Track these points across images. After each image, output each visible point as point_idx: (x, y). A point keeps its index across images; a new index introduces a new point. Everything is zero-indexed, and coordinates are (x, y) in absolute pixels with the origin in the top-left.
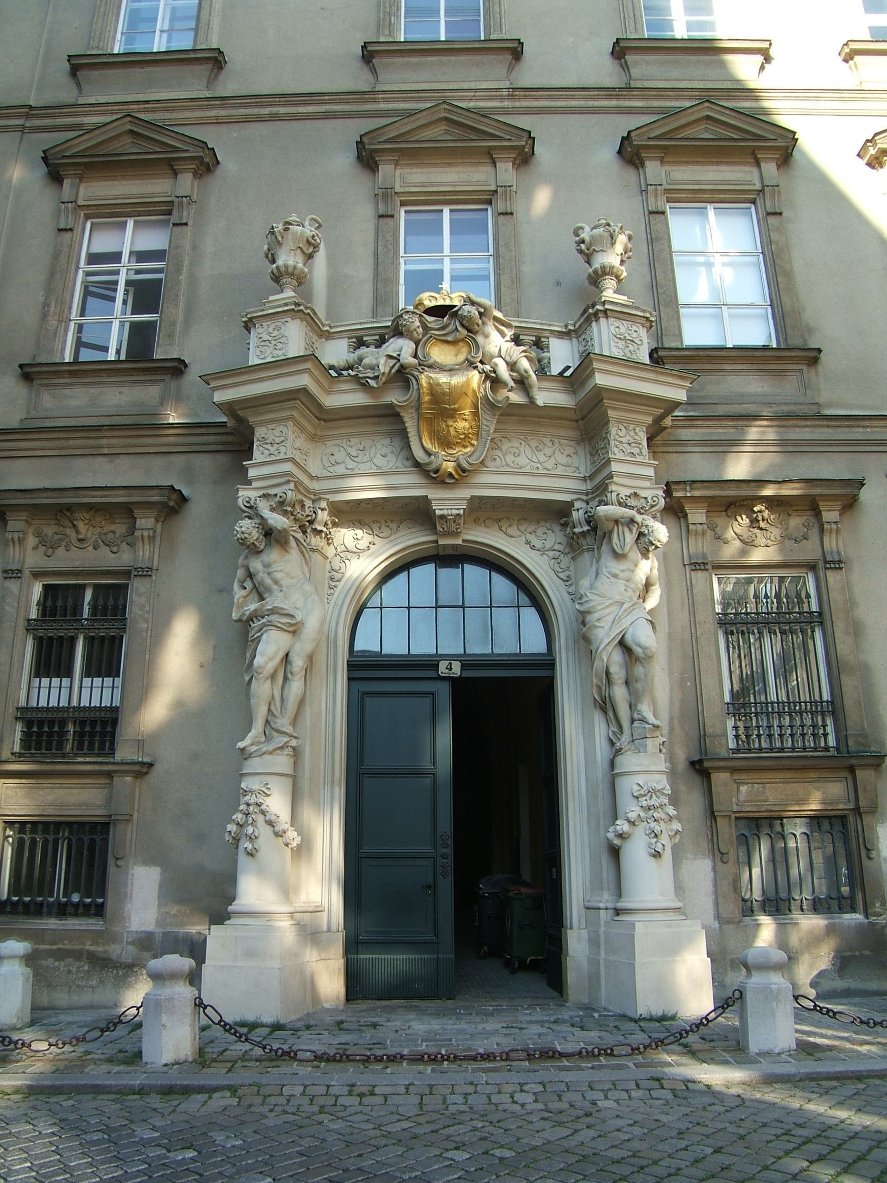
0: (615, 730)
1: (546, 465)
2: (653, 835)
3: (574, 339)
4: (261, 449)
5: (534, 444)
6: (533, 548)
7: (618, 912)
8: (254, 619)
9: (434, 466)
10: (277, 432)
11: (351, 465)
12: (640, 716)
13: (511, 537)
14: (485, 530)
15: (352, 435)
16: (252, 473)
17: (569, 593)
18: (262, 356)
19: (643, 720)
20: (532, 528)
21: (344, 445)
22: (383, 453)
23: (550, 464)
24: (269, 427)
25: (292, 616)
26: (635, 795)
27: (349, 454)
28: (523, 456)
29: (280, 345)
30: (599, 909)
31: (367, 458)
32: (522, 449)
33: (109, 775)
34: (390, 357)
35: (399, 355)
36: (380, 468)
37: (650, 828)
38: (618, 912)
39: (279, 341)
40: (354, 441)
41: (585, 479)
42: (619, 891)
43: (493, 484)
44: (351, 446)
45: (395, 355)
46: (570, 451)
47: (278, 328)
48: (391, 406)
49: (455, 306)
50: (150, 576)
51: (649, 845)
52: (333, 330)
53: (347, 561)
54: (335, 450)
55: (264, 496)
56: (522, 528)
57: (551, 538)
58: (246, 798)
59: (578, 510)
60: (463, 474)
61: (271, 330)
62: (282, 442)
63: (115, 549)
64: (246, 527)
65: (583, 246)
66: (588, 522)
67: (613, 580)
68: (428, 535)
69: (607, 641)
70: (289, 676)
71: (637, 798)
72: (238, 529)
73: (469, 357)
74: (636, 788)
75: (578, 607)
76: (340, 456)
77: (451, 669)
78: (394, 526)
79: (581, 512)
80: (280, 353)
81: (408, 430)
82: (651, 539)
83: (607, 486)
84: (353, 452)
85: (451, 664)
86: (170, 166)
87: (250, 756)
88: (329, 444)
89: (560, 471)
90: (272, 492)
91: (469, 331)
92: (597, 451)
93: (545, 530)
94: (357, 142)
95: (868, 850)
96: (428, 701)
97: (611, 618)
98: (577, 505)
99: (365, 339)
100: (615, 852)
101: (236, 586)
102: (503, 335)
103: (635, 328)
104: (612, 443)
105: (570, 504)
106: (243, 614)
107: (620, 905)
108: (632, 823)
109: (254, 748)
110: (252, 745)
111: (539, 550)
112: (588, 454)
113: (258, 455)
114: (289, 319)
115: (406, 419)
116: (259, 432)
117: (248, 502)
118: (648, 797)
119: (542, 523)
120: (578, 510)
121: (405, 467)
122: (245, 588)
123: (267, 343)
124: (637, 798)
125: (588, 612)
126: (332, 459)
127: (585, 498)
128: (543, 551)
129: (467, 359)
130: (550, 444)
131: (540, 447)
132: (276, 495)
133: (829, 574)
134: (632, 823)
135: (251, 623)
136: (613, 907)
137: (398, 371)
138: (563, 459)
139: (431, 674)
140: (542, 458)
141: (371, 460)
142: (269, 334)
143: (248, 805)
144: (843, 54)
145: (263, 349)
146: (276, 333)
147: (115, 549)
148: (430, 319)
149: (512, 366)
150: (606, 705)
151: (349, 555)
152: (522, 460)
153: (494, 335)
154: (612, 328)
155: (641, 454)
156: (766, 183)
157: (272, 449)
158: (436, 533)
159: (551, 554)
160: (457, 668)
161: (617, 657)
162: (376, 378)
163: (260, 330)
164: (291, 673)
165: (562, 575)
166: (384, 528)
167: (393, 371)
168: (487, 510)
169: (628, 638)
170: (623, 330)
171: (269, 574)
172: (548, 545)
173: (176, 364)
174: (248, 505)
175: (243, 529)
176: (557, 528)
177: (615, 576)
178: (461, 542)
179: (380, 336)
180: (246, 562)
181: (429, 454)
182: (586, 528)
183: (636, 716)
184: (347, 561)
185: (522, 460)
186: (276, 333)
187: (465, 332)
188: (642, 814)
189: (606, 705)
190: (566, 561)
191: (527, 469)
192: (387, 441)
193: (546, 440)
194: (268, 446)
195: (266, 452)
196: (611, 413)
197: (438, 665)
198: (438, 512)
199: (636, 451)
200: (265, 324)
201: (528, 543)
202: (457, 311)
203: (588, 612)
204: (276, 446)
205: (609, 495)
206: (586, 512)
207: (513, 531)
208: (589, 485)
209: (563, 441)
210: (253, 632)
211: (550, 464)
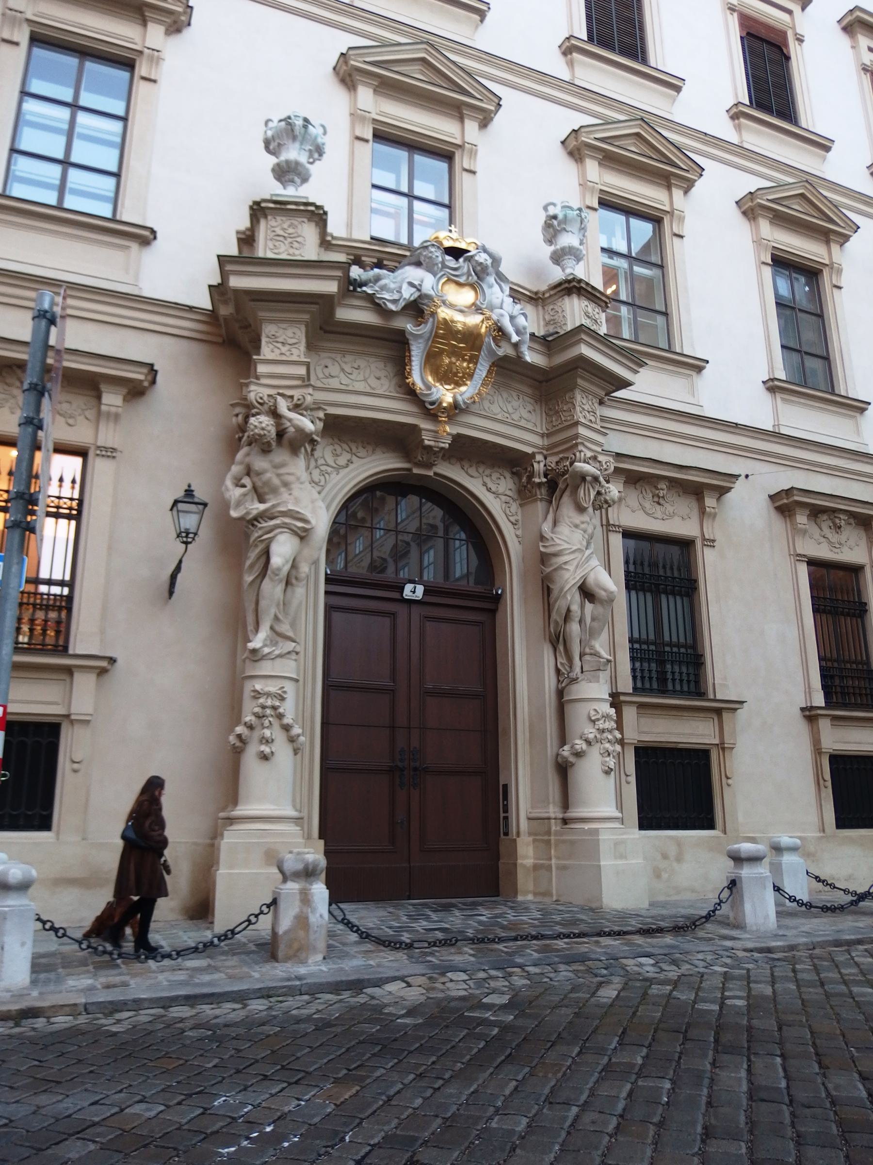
0: (565, 661)
1: (514, 416)
2: (607, 754)
3: (540, 308)
4: (271, 346)
5: (505, 395)
6: (489, 490)
7: (565, 821)
8: (260, 520)
9: (433, 398)
10: (289, 333)
11: (345, 381)
12: (592, 651)
13: (472, 477)
14: (449, 465)
15: (351, 352)
16: (261, 369)
17: (517, 536)
18: (276, 251)
19: (596, 654)
20: (488, 472)
21: (338, 359)
22: (377, 376)
23: (516, 417)
24: (280, 325)
25: (306, 521)
26: (593, 718)
27: (343, 370)
28: (496, 405)
29: (296, 245)
30: (549, 819)
31: (361, 377)
32: (496, 398)
33: (69, 671)
34: (411, 284)
35: (420, 285)
36: (373, 389)
37: (604, 748)
38: (565, 821)
39: (294, 240)
40: (349, 358)
41: (542, 436)
42: (566, 805)
43: (476, 427)
44: (346, 363)
45: (416, 283)
46: (530, 407)
47: (295, 227)
48: (402, 333)
49: (469, 251)
50: (114, 457)
51: (603, 763)
52: (334, 242)
53: (327, 475)
54: (329, 363)
55: (282, 395)
56: (481, 470)
57: (505, 484)
58: (261, 701)
59: (539, 462)
60: (456, 410)
61: (285, 226)
62: (295, 344)
63: (71, 421)
64: (262, 423)
65: (555, 222)
66: (546, 476)
67: (574, 529)
68: (396, 462)
69: (573, 582)
70: (294, 581)
71: (594, 722)
72: (256, 424)
73: (478, 303)
74: (592, 713)
75: (542, 549)
76: (334, 369)
77: (414, 592)
78: (370, 448)
79: (542, 464)
80: (297, 252)
81: (413, 358)
82: (608, 498)
83: (577, 445)
84: (347, 368)
85: (415, 588)
86: (457, 111)
87: (264, 657)
88: (323, 355)
89: (523, 423)
90: (289, 392)
91: (478, 278)
92: (557, 412)
93: (498, 475)
94: (342, 54)
95: (728, 778)
96: (387, 621)
97: (575, 563)
98: (539, 457)
99: (364, 259)
100: (563, 770)
101: (229, 483)
102: (502, 291)
103: (597, 310)
104: (578, 409)
105: (533, 455)
106: (248, 513)
107: (569, 815)
108: (589, 742)
109: (266, 650)
110: (265, 645)
111: (494, 493)
112: (544, 414)
113: (267, 351)
114: (305, 220)
115: (413, 348)
116: (268, 330)
117: (261, 398)
118: (602, 722)
119: (496, 469)
120: (539, 462)
121: (398, 393)
122: (244, 486)
123: (281, 239)
124: (594, 722)
125: (556, 555)
126: (326, 371)
127: (545, 452)
128: (496, 494)
129: (474, 304)
130: (516, 398)
131: (510, 399)
132: (292, 397)
133: (706, 549)
134: (589, 742)
135: (256, 523)
136: (561, 816)
137: (415, 301)
138: (525, 414)
139: (395, 595)
140: (511, 410)
141: (365, 380)
142: (284, 229)
143: (263, 707)
144: (564, 47)
145: (277, 244)
146: (291, 231)
147: (71, 421)
148: (448, 258)
149: (512, 318)
150: (558, 640)
151: (329, 469)
152: (495, 408)
153: (496, 288)
154: (583, 305)
155: (596, 423)
156: (466, 140)
157: (284, 349)
158: (409, 462)
159: (503, 498)
160: (420, 589)
161: (577, 597)
162: (394, 302)
163: (273, 223)
164: (297, 578)
165: (512, 519)
166: (361, 449)
167: (412, 299)
168: (468, 450)
169: (591, 581)
170: (590, 310)
171: (278, 475)
172: (501, 489)
173: (146, 233)
174: (261, 401)
175: (264, 425)
176: (508, 475)
177: (576, 526)
178: (431, 473)
179: (378, 259)
180: (247, 459)
181: (429, 387)
182: (544, 480)
183: (587, 650)
184: (327, 475)
185: (495, 408)
186: (291, 231)
187: (475, 278)
188: (598, 736)
189: (558, 640)
190: (514, 507)
191: (499, 417)
192: (381, 365)
193: (514, 394)
194: (279, 345)
195: (277, 351)
196: (580, 381)
197: (403, 589)
198: (427, 442)
199: (593, 419)
200: (278, 218)
201: (485, 484)
202: (472, 257)
203: (556, 555)
204: (288, 347)
205: (578, 454)
206: (545, 465)
207: (472, 471)
208: (546, 442)
209: (526, 398)
210: (260, 533)
211: (516, 417)
